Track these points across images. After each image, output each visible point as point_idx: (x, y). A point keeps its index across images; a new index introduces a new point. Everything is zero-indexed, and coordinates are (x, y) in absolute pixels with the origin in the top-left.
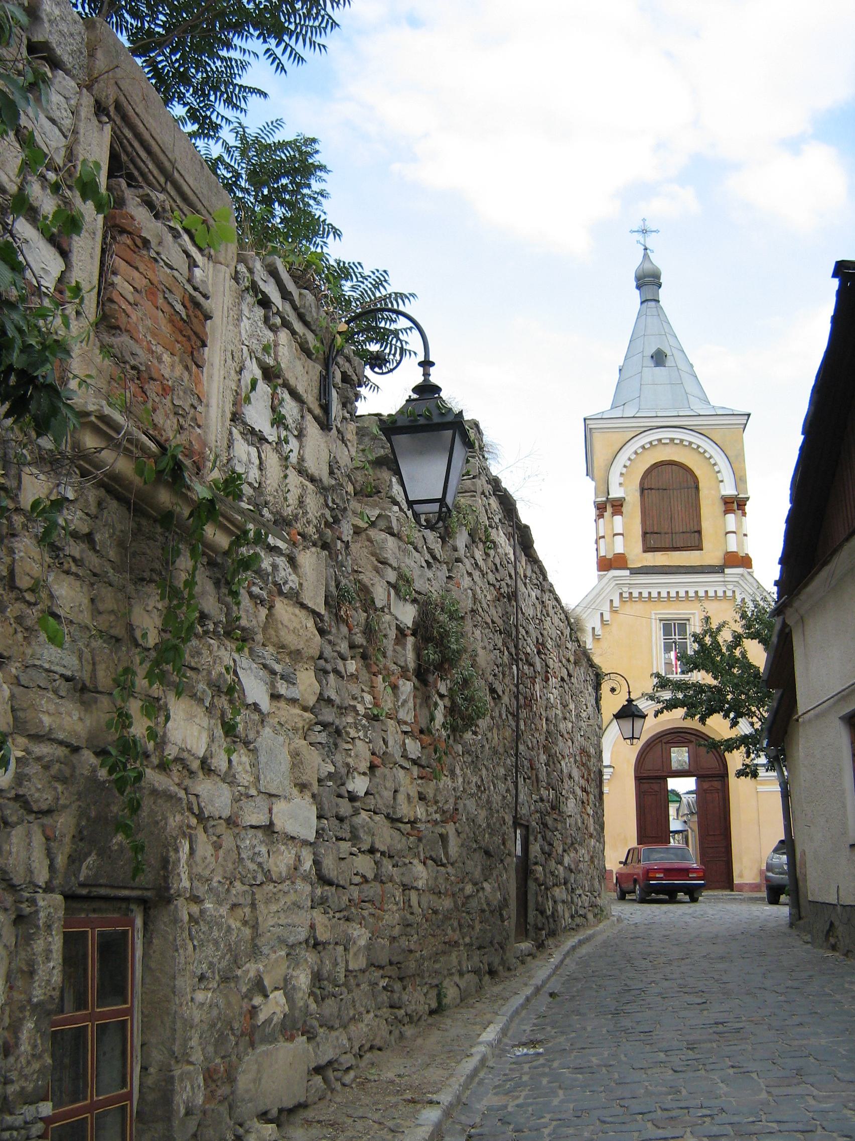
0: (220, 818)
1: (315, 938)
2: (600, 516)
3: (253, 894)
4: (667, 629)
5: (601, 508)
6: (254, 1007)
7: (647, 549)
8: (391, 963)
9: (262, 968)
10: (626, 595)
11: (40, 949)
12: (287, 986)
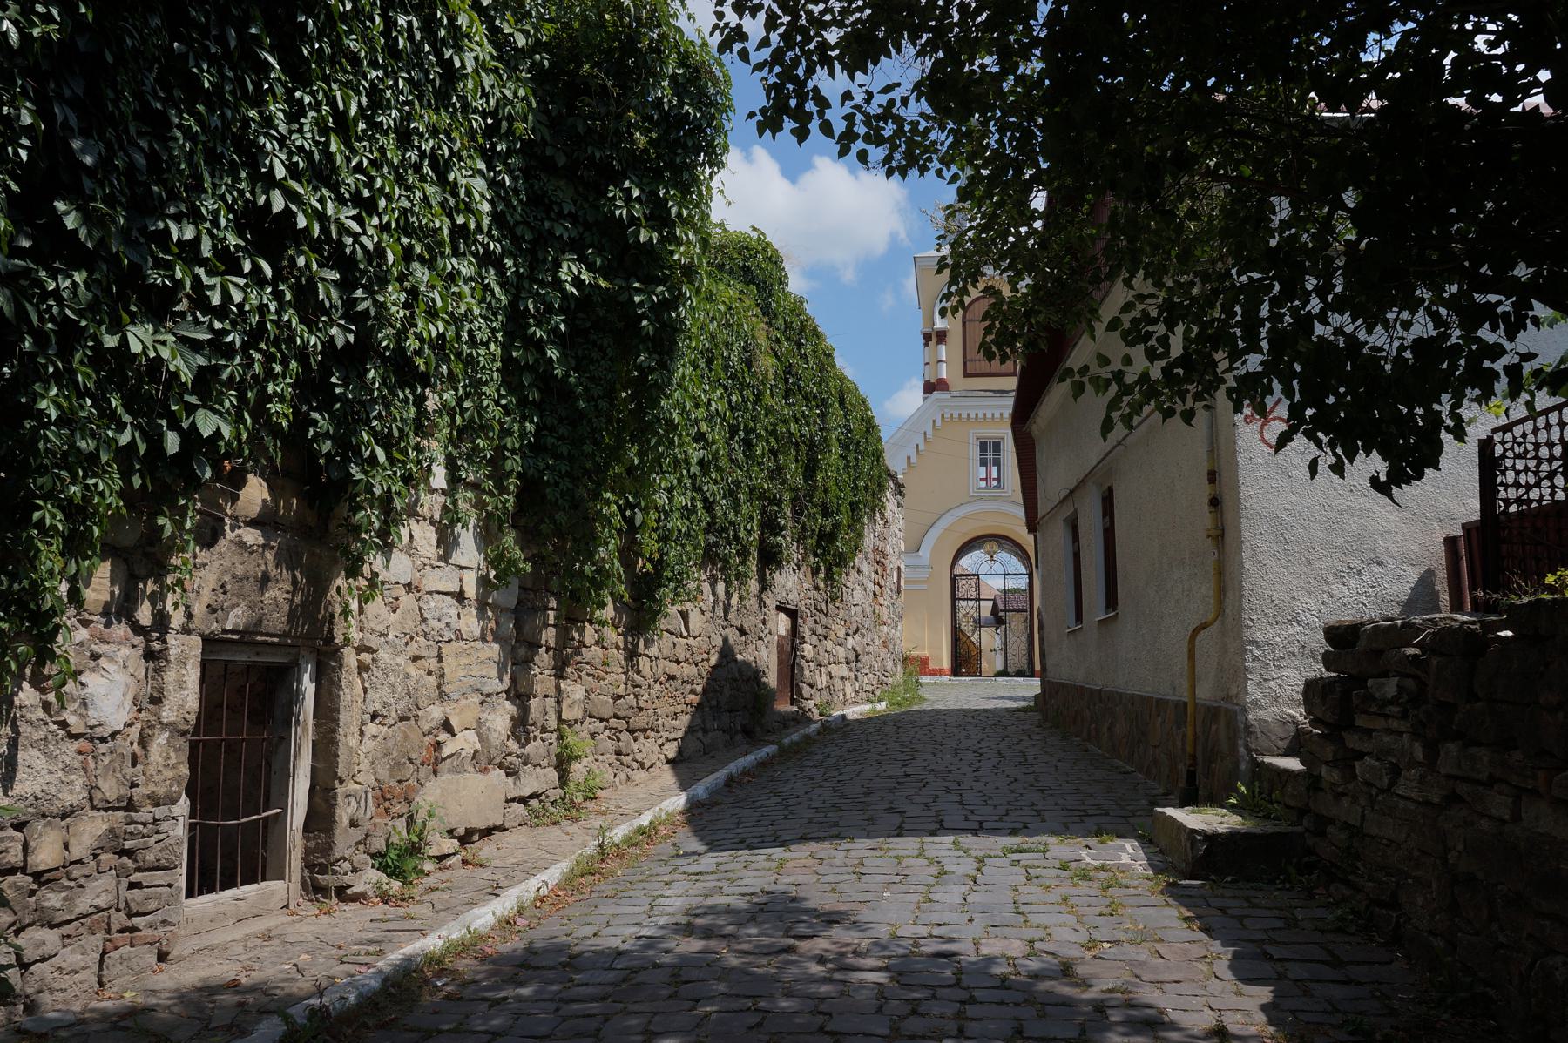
0: (397, 583)
1: (516, 691)
2: (926, 344)
3: (440, 648)
4: (983, 446)
5: (927, 338)
6: (439, 743)
7: (967, 375)
8: (616, 716)
9: (449, 711)
10: (947, 416)
11: (171, 679)
12: (479, 728)
